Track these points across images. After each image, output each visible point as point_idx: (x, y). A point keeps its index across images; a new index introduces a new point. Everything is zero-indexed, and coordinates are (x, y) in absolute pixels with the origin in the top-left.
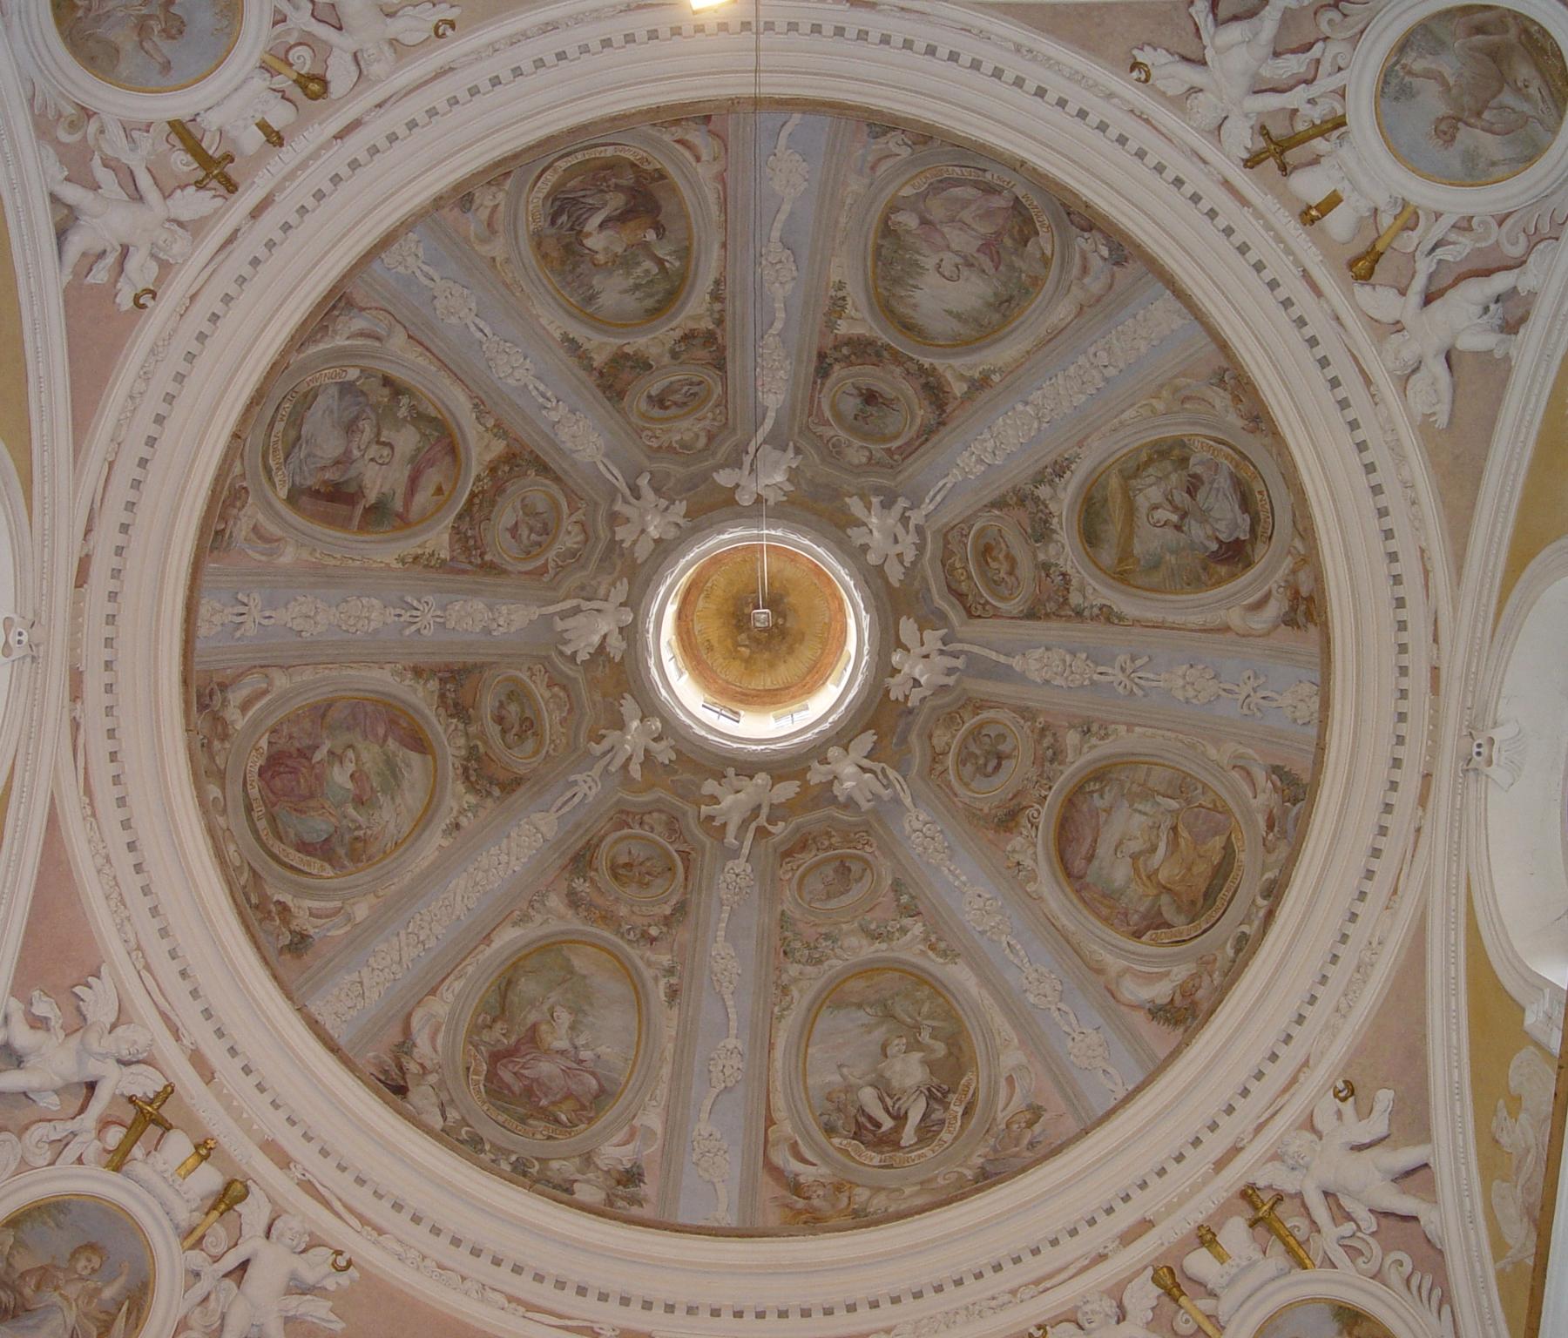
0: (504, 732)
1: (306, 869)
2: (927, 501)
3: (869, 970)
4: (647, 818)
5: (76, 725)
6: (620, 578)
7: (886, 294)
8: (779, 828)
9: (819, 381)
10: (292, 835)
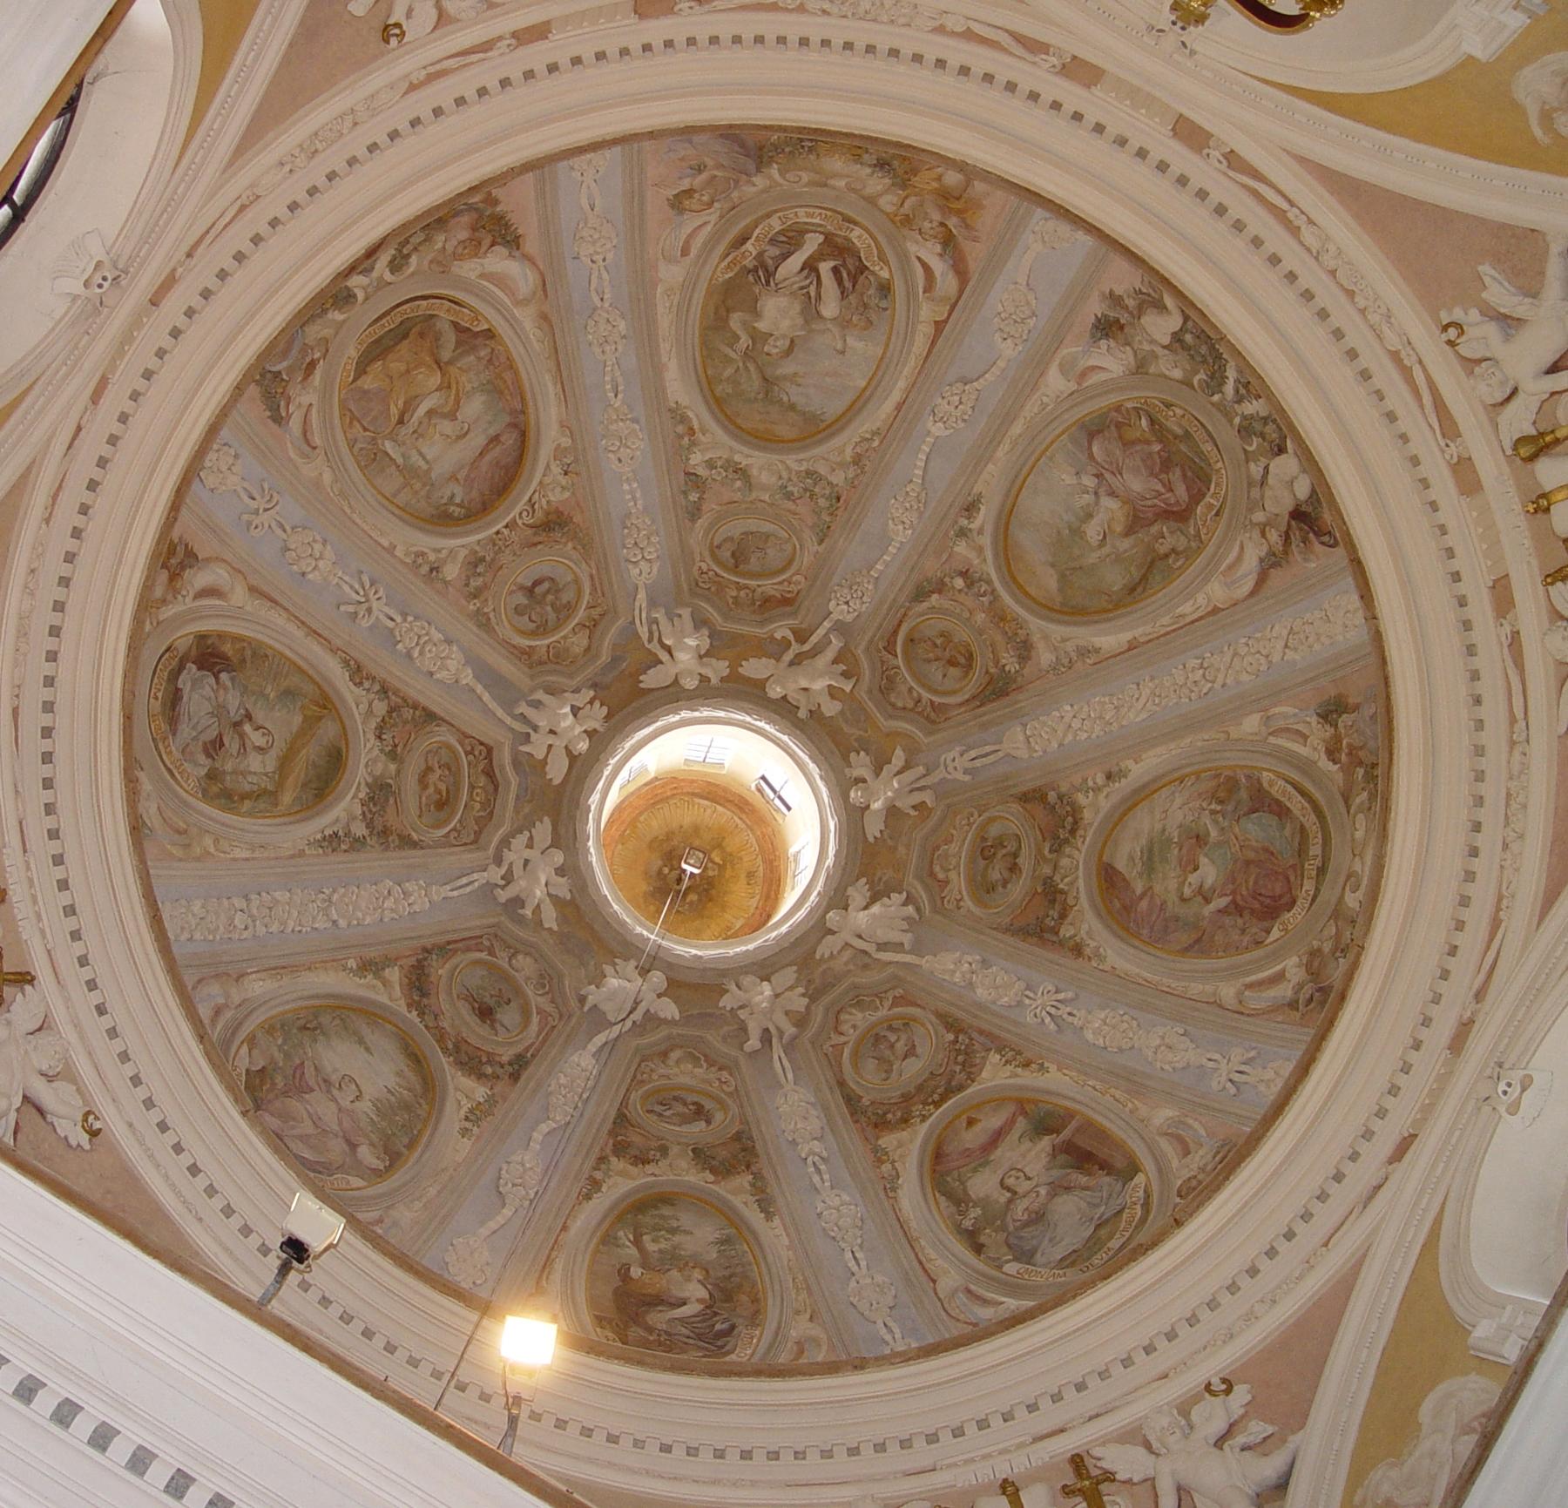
0: (1015, 855)
1: (1289, 788)
2: (476, 884)
3: (764, 440)
4: (910, 704)
5: (1479, 996)
6: (822, 960)
7: (421, 1101)
8: (782, 631)
9: (529, 1055)
10: (1287, 832)
